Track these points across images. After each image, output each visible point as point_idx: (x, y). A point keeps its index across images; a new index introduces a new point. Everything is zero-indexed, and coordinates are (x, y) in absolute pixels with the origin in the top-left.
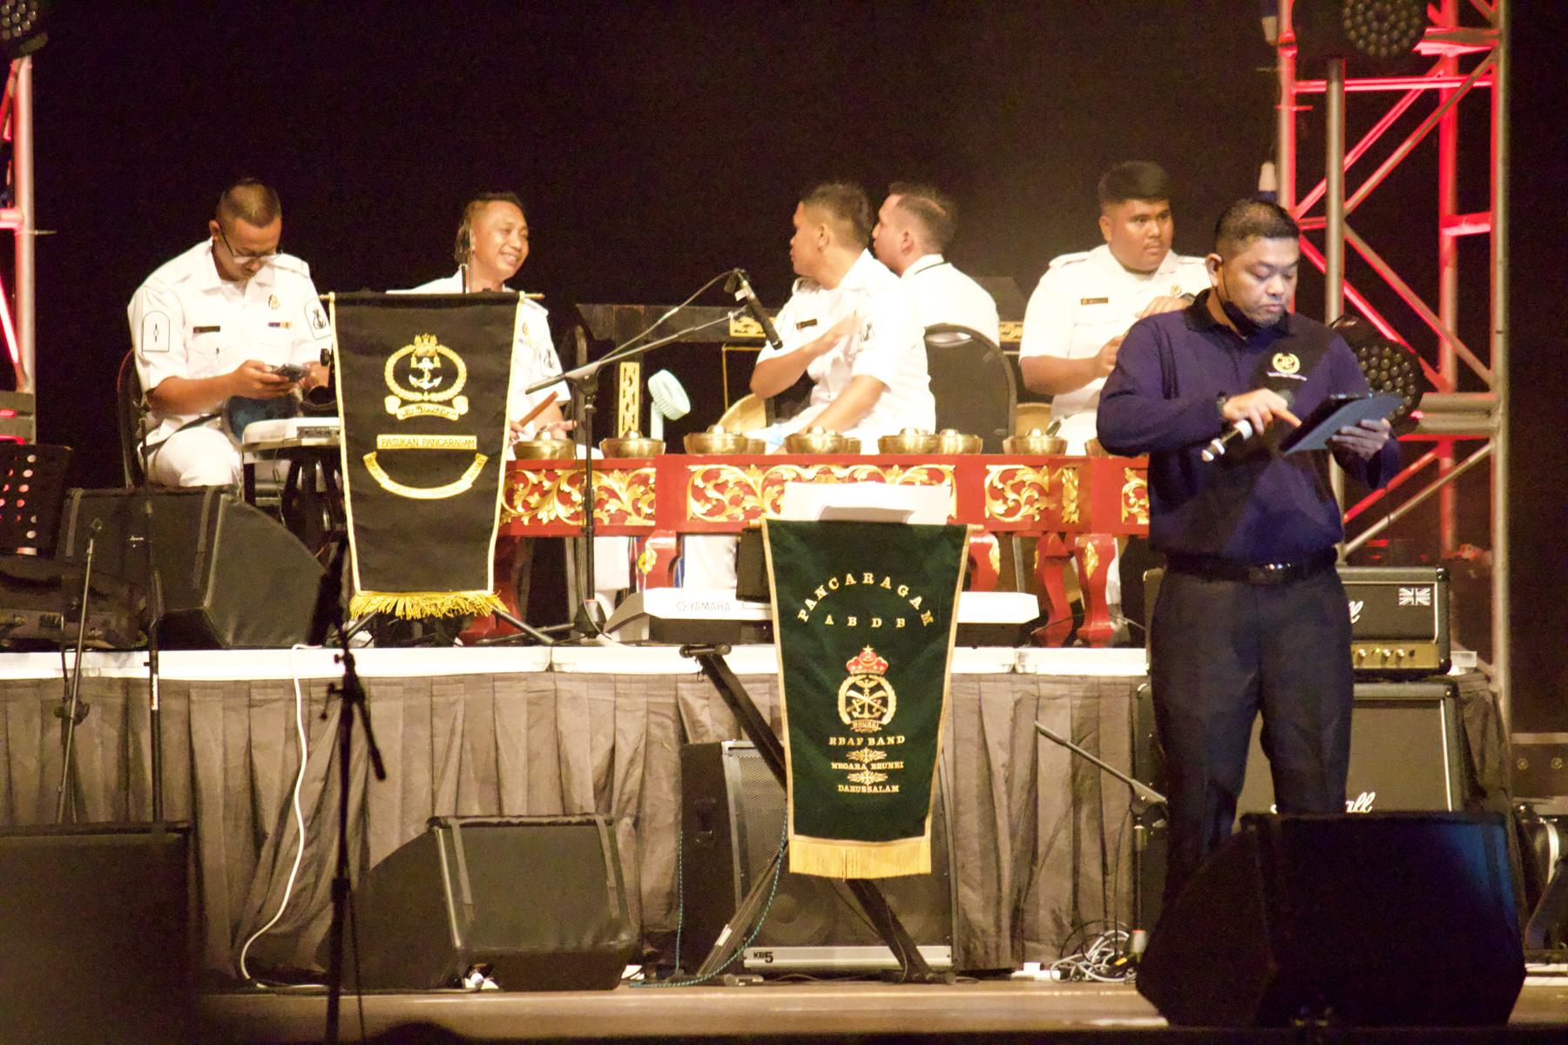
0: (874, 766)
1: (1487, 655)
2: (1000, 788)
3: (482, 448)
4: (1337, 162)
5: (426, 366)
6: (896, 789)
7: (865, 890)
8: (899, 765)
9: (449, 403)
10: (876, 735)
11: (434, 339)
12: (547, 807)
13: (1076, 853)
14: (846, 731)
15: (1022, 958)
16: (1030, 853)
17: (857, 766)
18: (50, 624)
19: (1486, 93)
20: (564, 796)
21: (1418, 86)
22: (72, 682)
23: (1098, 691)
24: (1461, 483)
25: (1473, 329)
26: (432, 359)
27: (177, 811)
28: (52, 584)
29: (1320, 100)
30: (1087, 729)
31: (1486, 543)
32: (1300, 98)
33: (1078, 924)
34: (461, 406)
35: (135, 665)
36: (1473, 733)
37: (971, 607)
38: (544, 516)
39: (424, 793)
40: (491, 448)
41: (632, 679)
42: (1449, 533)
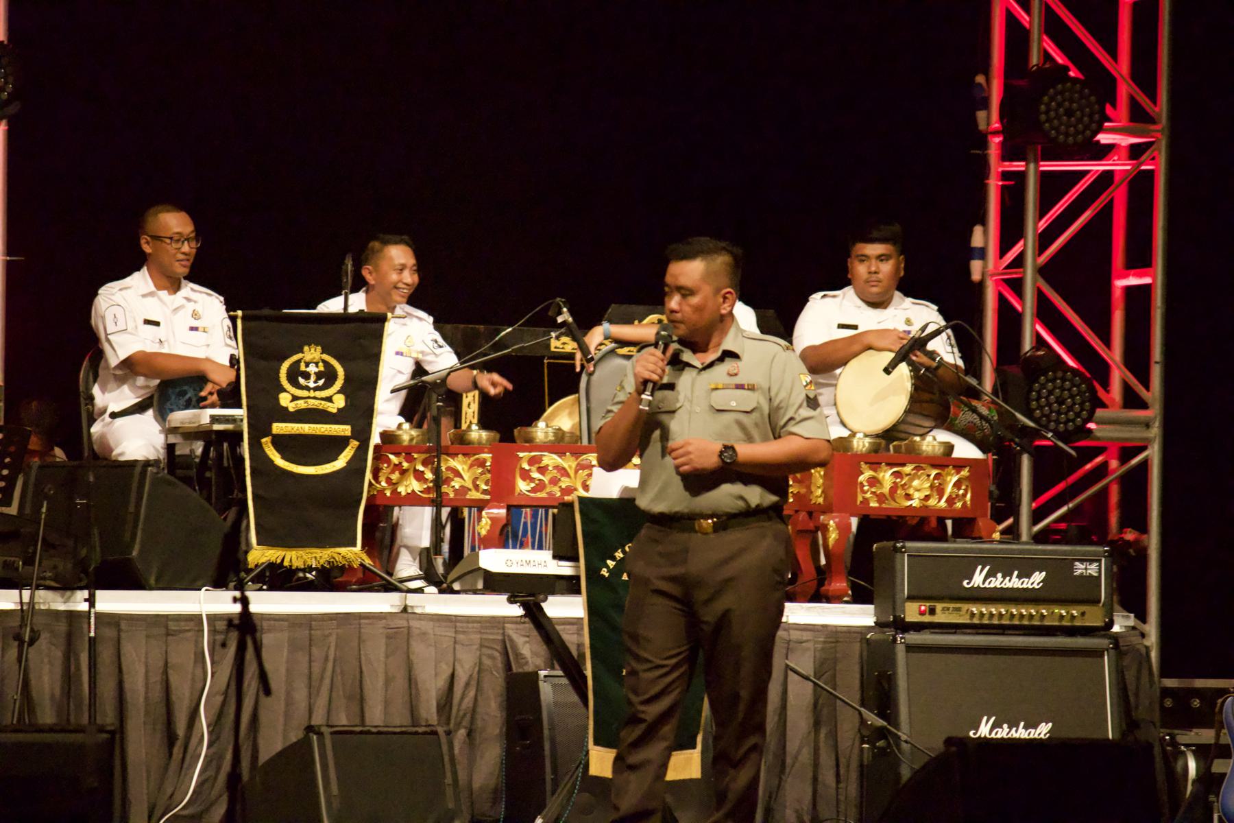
3: (355, 435)
4: (1033, 226)
5: (312, 369)
9: (329, 399)
11: (319, 349)
12: (400, 719)
13: (816, 765)
20: (413, 710)
21: (1097, 167)
22: (26, 613)
26: (317, 364)
27: (108, 716)
29: (1021, 177)
30: (826, 667)
31: (1144, 528)
34: (340, 402)
36: (1130, 676)
40: (362, 434)
42: (1114, 519)
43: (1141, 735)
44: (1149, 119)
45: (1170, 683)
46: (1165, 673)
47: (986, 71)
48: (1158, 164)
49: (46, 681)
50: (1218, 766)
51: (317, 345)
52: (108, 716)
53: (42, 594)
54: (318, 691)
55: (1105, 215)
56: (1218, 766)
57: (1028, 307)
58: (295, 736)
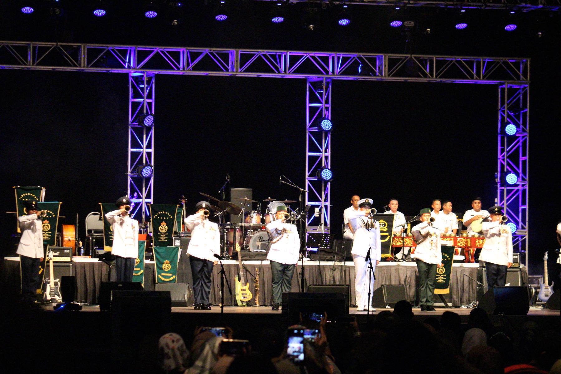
1: (525, 265)
2: (459, 282)
4: (505, 198)
7: (440, 296)
12: (397, 283)
13: (469, 291)
14: (438, 274)
15: (461, 305)
16: (463, 291)
18: (331, 258)
19: (525, 190)
20: (400, 282)
21: (516, 188)
22: (334, 266)
23: (472, 269)
24: (521, 242)
25: (524, 221)
27: (348, 283)
28: (332, 252)
29: (503, 190)
30: (471, 274)
31: (525, 250)
32: (501, 190)
33: (469, 301)
34: (386, 229)
35: (342, 263)
36: (523, 275)
37: (455, 257)
38: (397, 244)
39: (381, 281)
40: (390, 235)
41: (409, 266)
42: (520, 248)
43: (525, 285)
44: (525, 180)
45: (530, 276)
46: (529, 275)
47: (497, 172)
48: (527, 187)
49: (337, 277)
50: (538, 290)
52: (348, 283)
53: (336, 262)
55: (518, 197)
56: (538, 290)
57: (505, 164)
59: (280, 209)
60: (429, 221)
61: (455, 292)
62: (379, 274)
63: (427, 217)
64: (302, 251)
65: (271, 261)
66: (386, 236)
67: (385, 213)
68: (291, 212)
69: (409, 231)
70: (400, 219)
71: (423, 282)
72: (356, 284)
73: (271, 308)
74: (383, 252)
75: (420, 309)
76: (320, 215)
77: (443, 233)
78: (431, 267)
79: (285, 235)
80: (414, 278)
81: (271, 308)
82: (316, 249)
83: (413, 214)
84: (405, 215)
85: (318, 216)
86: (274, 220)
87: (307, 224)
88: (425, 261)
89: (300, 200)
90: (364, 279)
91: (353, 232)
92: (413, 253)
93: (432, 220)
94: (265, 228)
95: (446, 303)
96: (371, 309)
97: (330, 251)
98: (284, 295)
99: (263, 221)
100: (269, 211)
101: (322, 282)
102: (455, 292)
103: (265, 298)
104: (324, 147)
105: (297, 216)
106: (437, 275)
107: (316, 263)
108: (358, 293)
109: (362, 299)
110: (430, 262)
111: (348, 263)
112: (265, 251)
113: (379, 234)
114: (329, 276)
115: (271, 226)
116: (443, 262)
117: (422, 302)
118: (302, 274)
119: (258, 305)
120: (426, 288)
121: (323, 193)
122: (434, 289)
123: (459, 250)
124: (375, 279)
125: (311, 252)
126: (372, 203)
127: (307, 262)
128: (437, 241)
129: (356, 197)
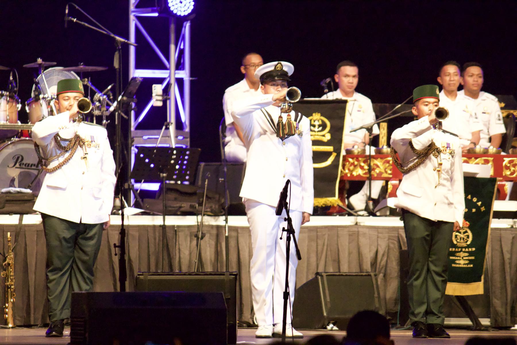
0: (464, 258)
2: (507, 266)
3: (335, 151)
6: (472, 266)
7: (461, 299)
8: (473, 258)
9: (324, 136)
10: (465, 248)
11: (319, 114)
12: (355, 270)
14: (455, 246)
17: (459, 258)
20: (360, 266)
22: (200, 226)
26: (318, 121)
27: (234, 269)
28: (194, 194)
34: (328, 137)
35: (221, 221)
37: (498, 206)
38: (355, 174)
40: (338, 150)
49: (208, 254)
51: (318, 113)
54: (321, 258)
58: (311, 277)
59: (65, 87)
60: (433, 116)
61: (498, 292)
62: (309, 246)
63: (431, 106)
64: (121, 190)
65: (44, 216)
66: (327, 155)
67: (324, 98)
68: (93, 94)
69: (383, 140)
70: (360, 111)
71: (419, 266)
72: (253, 271)
73: (43, 332)
74: (318, 193)
75: (410, 333)
76: (165, 102)
77: (467, 144)
78: (437, 228)
79: (79, 152)
80: (395, 255)
81: (43, 332)
82: (154, 187)
83: (394, 97)
84: (373, 102)
85: (160, 104)
86: (51, 113)
87: (133, 124)
88: (423, 216)
89: (116, 65)
90: (272, 260)
91: (247, 142)
92: (394, 194)
93: (441, 114)
94: (29, 134)
95: (474, 319)
96: (290, 332)
97: (190, 190)
98: (76, 300)
99: (24, 117)
100: (39, 91)
101: (171, 266)
102: (498, 292)
103: (29, 305)
104: (174, 55)
105: (109, 106)
106: (452, 249)
107: (157, 221)
108: (260, 293)
109: (268, 307)
110: (434, 217)
111: (235, 221)
112: (28, 191)
113: (309, 149)
114: (187, 253)
115: (42, 129)
116: (467, 217)
117: (415, 315)
118: (122, 246)
119: (10, 325)
120: (426, 279)
121: (172, 47)
122: (445, 282)
123: (508, 187)
124: (299, 258)
125: (145, 194)
126: (290, 73)
127: (133, 217)
128: (452, 164)
129: (254, 59)
